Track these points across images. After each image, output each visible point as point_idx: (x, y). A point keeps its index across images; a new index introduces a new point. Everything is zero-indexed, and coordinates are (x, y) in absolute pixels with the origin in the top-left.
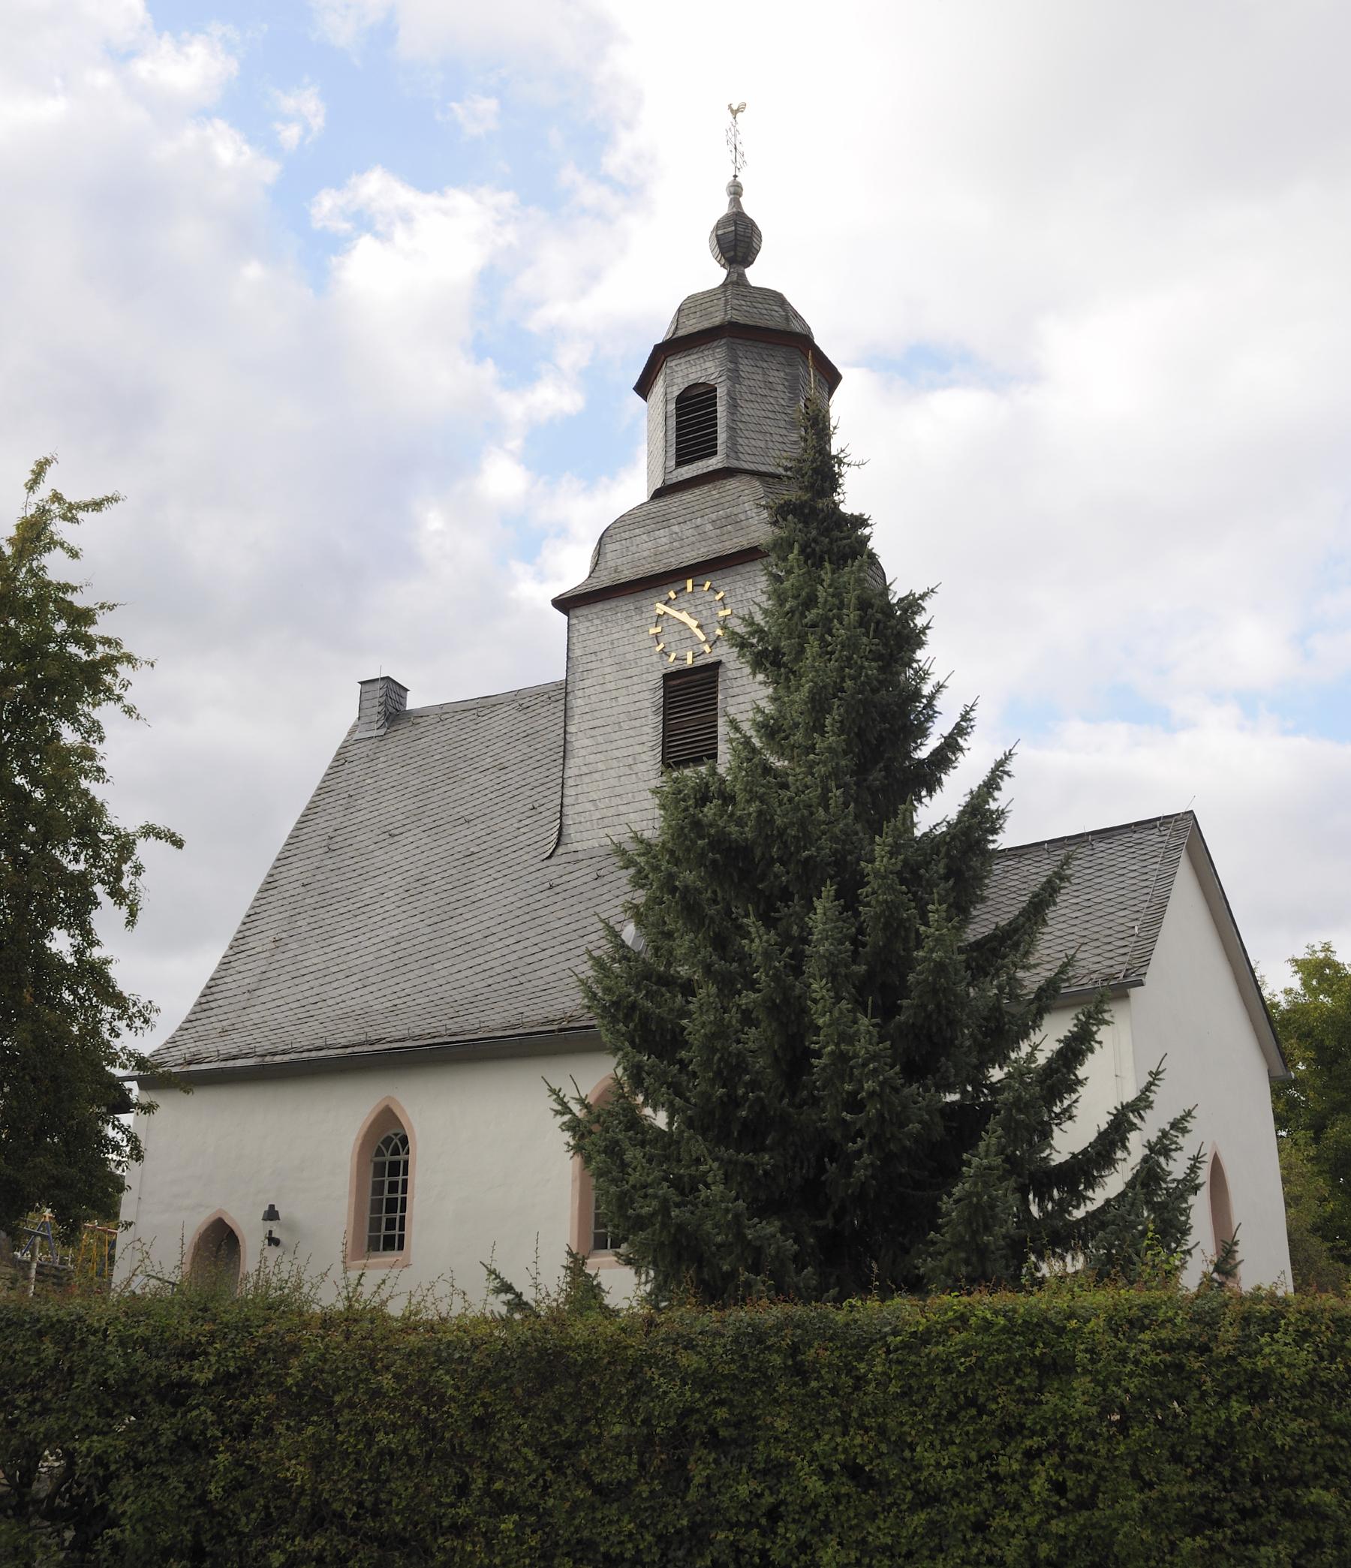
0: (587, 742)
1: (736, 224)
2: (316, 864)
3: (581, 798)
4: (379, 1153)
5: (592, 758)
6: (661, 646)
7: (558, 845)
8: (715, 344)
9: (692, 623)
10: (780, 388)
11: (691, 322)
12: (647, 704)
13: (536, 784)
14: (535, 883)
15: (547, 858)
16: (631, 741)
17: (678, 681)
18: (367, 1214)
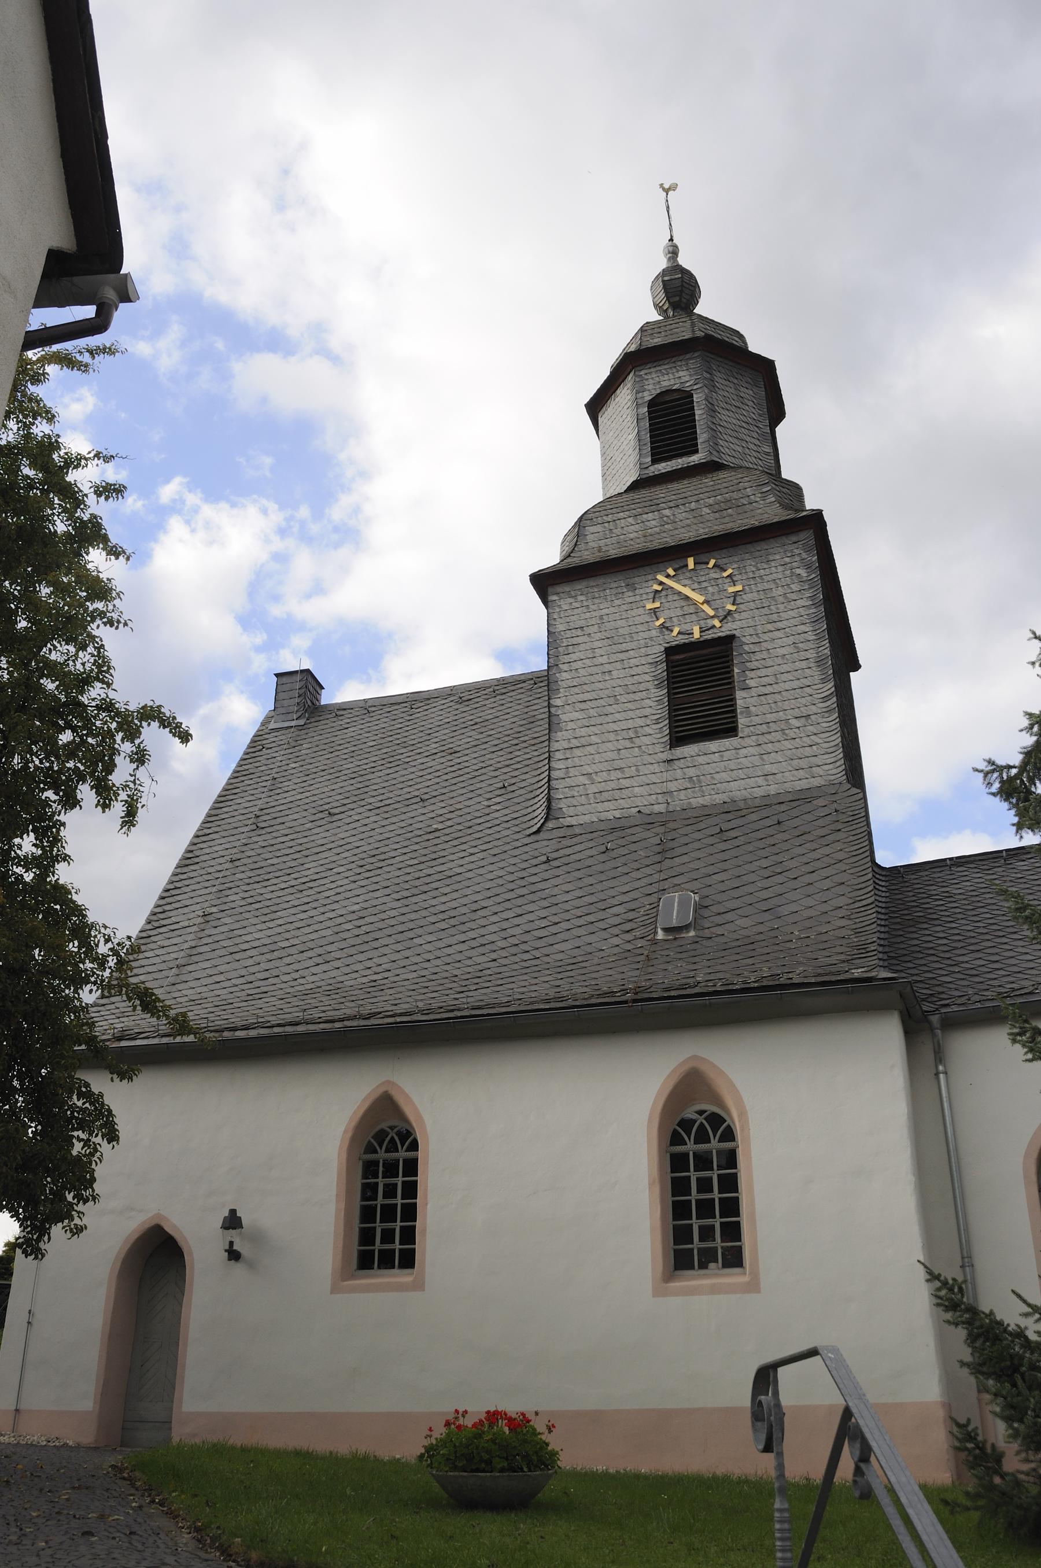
0: (577, 715)
2: (244, 841)
3: (573, 772)
4: (370, 1149)
5: (584, 732)
6: (661, 621)
7: (546, 820)
8: (688, 356)
9: (699, 598)
10: (750, 403)
15: (534, 833)
16: (631, 714)
17: (682, 656)
18: (356, 1225)
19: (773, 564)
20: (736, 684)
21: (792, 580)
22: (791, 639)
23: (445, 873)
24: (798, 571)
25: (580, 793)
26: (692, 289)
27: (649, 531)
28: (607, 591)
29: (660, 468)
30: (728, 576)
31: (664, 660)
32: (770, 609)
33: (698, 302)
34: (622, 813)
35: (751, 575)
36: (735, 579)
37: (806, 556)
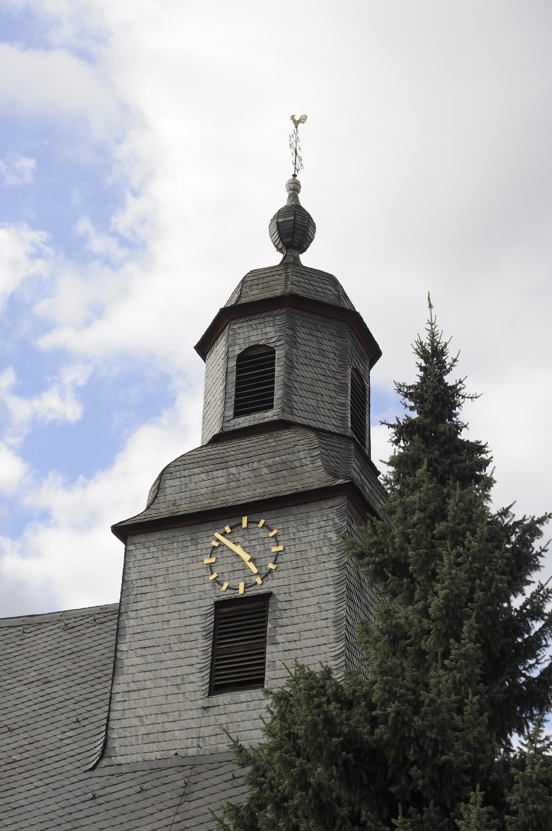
0: (137, 660)
1: (295, 215)
3: (128, 714)
5: (141, 676)
6: (215, 575)
7: (102, 757)
8: (276, 312)
9: (246, 557)
10: (331, 355)
11: (254, 292)
12: (198, 628)
13: (80, 698)
14: (78, 793)
16: (180, 662)
19: (311, 527)
20: (267, 639)
21: (324, 542)
22: (316, 600)
23: (11, 805)
24: (330, 535)
25: (132, 734)
26: (305, 229)
27: (217, 487)
28: (175, 544)
29: (240, 422)
30: (273, 536)
31: (213, 612)
32: (303, 570)
33: (314, 237)
34: (163, 755)
35: (292, 537)
36: (279, 539)
37: (338, 521)
